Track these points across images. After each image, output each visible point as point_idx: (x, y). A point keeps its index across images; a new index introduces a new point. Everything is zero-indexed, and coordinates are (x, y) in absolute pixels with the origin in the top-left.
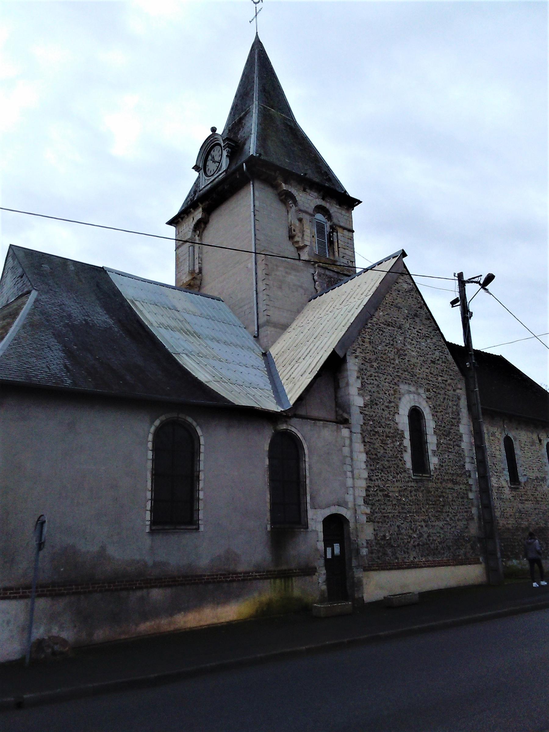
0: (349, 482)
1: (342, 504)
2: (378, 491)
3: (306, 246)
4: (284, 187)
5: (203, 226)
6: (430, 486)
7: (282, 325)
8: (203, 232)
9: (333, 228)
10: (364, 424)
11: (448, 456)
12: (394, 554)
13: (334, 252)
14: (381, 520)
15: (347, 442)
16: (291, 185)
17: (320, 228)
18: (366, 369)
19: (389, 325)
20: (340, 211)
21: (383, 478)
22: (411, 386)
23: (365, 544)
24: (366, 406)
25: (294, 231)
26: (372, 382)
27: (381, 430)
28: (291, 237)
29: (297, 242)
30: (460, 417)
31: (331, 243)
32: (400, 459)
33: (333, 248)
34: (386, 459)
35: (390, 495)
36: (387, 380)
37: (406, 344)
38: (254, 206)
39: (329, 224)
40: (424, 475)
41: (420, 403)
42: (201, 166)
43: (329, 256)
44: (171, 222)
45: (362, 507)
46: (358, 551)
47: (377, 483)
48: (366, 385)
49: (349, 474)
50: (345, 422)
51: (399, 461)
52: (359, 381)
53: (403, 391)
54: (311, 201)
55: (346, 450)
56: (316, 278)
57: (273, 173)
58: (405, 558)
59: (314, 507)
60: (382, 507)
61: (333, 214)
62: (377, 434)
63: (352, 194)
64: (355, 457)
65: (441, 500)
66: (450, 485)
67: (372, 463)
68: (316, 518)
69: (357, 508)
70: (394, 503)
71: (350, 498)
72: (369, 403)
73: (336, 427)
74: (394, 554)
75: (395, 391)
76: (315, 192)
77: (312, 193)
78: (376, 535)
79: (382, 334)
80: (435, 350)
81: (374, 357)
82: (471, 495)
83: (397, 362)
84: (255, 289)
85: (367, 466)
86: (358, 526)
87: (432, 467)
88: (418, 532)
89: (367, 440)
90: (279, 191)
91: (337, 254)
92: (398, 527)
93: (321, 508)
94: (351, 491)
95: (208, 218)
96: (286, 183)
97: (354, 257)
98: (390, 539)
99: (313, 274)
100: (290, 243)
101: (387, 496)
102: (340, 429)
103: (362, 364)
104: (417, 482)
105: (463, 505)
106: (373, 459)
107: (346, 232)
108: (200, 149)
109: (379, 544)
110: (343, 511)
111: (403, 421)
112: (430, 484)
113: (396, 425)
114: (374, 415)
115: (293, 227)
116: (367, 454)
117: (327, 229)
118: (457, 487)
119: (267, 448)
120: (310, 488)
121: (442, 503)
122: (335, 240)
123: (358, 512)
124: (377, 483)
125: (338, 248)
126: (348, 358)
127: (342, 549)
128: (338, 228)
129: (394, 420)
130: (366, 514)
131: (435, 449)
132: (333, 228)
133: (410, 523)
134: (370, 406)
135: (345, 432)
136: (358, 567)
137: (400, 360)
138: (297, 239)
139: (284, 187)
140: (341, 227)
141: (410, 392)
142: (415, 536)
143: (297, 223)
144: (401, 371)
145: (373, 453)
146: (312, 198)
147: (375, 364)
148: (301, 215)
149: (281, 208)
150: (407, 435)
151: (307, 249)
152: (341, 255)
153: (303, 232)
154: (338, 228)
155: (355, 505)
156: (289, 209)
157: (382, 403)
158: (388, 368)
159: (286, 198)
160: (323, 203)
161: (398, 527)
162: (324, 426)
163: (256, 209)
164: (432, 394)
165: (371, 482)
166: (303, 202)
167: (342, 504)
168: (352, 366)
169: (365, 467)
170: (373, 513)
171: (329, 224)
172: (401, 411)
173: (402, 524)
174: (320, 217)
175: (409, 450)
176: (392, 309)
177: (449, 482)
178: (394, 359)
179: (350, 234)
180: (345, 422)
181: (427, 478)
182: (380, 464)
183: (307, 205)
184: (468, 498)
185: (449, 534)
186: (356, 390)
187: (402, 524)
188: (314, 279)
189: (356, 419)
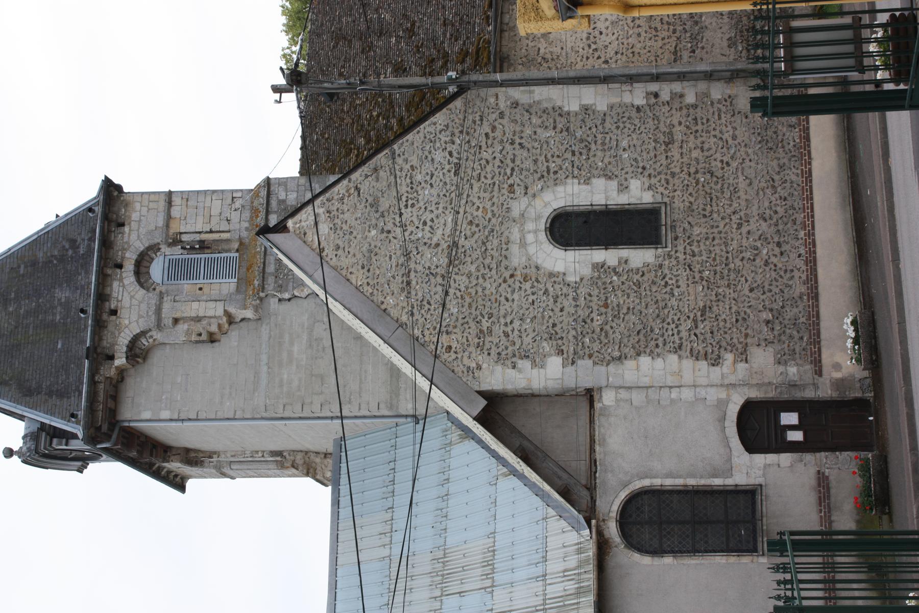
0: (687, 394)
1: (722, 405)
2: (697, 332)
3: (225, 311)
4: (120, 361)
5: (193, 455)
6: (682, 205)
7: (391, 376)
8: (202, 452)
9: (175, 241)
10: (590, 356)
11: (624, 150)
12: (794, 302)
13: (222, 241)
14: (743, 329)
15: (623, 394)
16: (113, 345)
17: (177, 270)
18: (497, 346)
19: (409, 283)
20: (134, 225)
21: (676, 318)
22: (512, 238)
23: (781, 369)
24: (561, 352)
25: (200, 335)
26: (516, 332)
27: (598, 320)
28: (212, 339)
29: (220, 326)
30: (548, 105)
31: (203, 246)
32: (642, 276)
33: (214, 241)
34: (644, 310)
35: (701, 304)
36: (509, 296)
37: (435, 240)
38: (171, 420)
39: (164, 249)
40: (664, 223)
41: (538, 218)
42: (79, 464)
43: (229, 251)
44: (181, 488)
45: (725, 370)
46: (793, 385)
47: (684, 334)
48: (524, 346)
49: (674, 394)
50: (590, 395)
51: (645, 278)
52: (520, 363)
53: (524, 259)
54: (132, 297)
55: (637, 397)
56: (287, 296)
57: (101, 386)
58: (800, 277)
59: (729, 472)
60: (722, 324)
61: (147, 245)
62: (603, 329)
63: (90, 191)
64: (646, 381)
65: (702, 179)
66: (675, 152)
67: (653, 343)
68: (748, 468)
69: (726, 382)
70: (714, 298)
71: (713, 395)
72: (555, 343)
73: (603, 419)
74: (794, 302)
75: (526, 278)
76: (111, 286)
77: (115, 295)
78: (768, 343)
79: (429, 303)
80: (433, 160)
81: (472, 324)
82: (690, 99)
83: (473, 268)
84: (329, 421)
85: (658, 355)
86: (754, 382)
87: (647, 198)
88: (758, 244)
89: (616, 354)
90: (129, 366)
91: (225, 236)
92: (751, 290)
93: (729, 460)
94: (702, 393)
95: (178, 448)
96: (111, 358)
97: (223, 191)
98: (771, 310)
99: (280, 300)
100: (224, 339)
101: (703, 311)
102: (605, 408)
103: (489, 354)
104: (676, 238)
105: (708, 120)
106: (646, 343)
107: (176, 212)
108: (47, 468)
109: (780, 335)
110: (733, 410)
111: (574, 263)
112: (677, 203)
113: (585, 282)
114: (574, 333)
115: (194, 338)
116: (639, 354)
117: (176, 252)
118: (678, 137)
119: (647, 560)
120: (701, 477)
121: (708, 176)
122: (198, 237)
123: (732, 379)
124: (684, 334)
125: (211, 232)
126: (485, 387)
127: (789, 406)
128: (172, 231)
129: (576, 287)
130: (735, 362)
131: (614, 184)
132: (175, 241)
133: (745, 262)
134: (560, 342)
135: (608, 398)
136: (816, 387)
137: (469, 259)
138: (214, 328)
139: (120, 361)
140: (167, 226)
141: (523, 244)
142: (765, 252)
143: (182, 327)
144: (487, 261)
145: (637, 339)
146: (125, 294)
147: (485, 324)
148: (168, 321)
149: (156, 358)
150: (599, 255)
151: (232, 310)
152: (224, 226)
153: (198, 319)
154: (172, 231)
155: (722, 385)
156: (157, 342)
157: (551, 314)
158: (487, 292)
159: (138, 353)
160: (129, 267)
161: (751, 290)
162: (603, 442)
163: (176, 417)
164: (517, 181)
165: (683, 348)
166: (140, 316)
167: (722, 405)
168: (499, 378)
169: (660, 360)
170: (732, 347)
171: (164, 249)
172: (559, 267)
173: (746, 281)
174: (157, 270)
175: (625, 253)
176: (378, 272)
177: (669, 154)
178: (469, 275)
179: (176, 200)
180: (590, 395)
181: (668, 208)
182: (653, 324)
183: (144, 306)
184: (695, 106)
185: (760, 166)
186: (535, 371)
187: (746, 281)
188: (289, 300)
189: (585, 374)
